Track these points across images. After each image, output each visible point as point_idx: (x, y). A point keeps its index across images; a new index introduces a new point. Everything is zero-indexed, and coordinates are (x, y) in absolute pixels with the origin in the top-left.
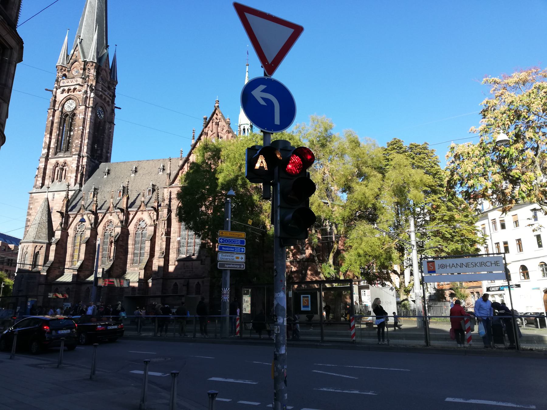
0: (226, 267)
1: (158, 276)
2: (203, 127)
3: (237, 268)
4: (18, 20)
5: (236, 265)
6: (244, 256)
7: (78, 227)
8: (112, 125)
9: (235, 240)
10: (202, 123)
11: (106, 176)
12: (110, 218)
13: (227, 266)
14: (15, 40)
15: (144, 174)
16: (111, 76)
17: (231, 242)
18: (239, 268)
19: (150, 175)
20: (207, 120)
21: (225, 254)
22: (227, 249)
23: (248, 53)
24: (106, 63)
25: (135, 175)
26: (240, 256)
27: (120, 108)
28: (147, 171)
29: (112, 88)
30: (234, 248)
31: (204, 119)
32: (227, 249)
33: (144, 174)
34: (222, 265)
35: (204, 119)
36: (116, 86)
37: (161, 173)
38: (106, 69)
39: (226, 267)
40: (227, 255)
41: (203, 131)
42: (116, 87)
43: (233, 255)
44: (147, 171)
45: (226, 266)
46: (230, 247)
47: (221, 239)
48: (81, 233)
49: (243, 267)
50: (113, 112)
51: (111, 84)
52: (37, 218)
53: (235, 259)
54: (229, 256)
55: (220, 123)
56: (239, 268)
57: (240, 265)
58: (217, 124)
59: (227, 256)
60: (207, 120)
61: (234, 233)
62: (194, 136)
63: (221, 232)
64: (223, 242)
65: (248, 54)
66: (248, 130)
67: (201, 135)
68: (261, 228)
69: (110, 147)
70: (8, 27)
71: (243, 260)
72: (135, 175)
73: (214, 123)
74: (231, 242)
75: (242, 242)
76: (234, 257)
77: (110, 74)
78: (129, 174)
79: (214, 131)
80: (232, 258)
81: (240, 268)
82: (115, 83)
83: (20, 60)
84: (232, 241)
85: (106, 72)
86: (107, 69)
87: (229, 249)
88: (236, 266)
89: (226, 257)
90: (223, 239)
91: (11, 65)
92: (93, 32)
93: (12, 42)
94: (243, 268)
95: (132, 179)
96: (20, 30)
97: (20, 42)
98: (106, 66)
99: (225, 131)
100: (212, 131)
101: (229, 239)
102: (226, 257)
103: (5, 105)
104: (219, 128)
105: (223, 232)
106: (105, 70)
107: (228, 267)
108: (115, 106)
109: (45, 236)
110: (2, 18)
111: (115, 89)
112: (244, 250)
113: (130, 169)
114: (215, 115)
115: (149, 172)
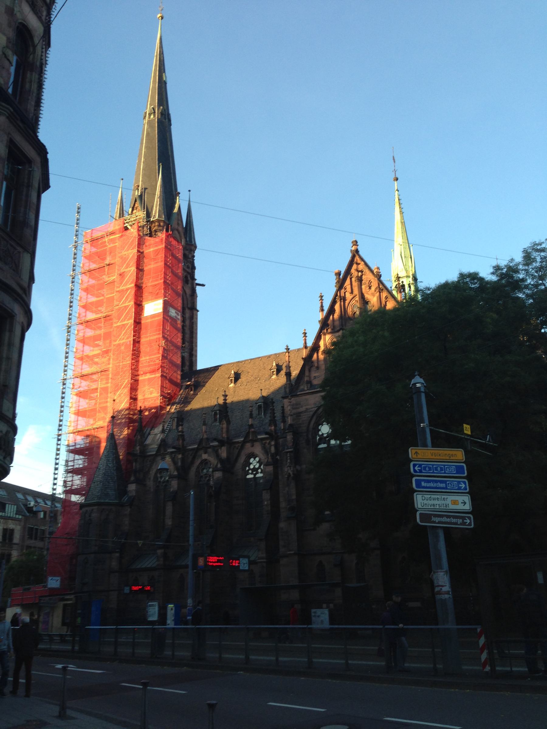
0: (434, 522)
1: (290, 551)
2: (334, 289)
3: (456, 524)
4: (40, 123)
5: (454, 517)
6: (467, 499)
7: (159, 475)
8: (195, 312)
9: (444, 465)
10: (333, 280)
11: (192, 392)
12: (205, 456)
13: (437, 520)
14: (34, 148)
15: (248, 382)
16: (186, 238)
17: (441, 468)
18: (461, 524)
19: (257, 382)
20: (341, 276)
21: (429, 496)
22: (432, 485)
23: (394, 159)
24: (178, 220)
25: (235, 385)
26: (460, 498)
27: (203, 285)
28: (252, 376)
29: (190, 256)
30: (445, 482)
31: (336, 274)
32: (432, 485)
33: (248, 382)
34: (426, 517)
35: (336, 274)
36: (194, 253)
37: (274, 377)
38: (179, 228)
39: (434, 522)
40: (433, 496)
41: (336, 295)
42: (195, 254)
43: (446, 497)
44: (252, 376)
45: (434, 519)
46: (436, 482)
47: (417, 464)
48: (164, 484)
49: (470, 522)
50: (193, 294)
51: (187, 250)
52: (101, 466)
53: (450, 505)
54: (438, 499)
55: (364, 277)
56: (461, 524)
57: (463, 518)
58: (360, 280)
59: (434, 499)
60: (341, 276)
61: (440, 452)
62: (322, 306)
63: (414, 451)
64: (420, 471)
65: (394, 162)
66: (410, 287)
67: (334, 302)
68: (489, 441)
69: (194, 347)
70: (21, 125)
71: (468, 507)
72: (235, 385)
73: (353, 279)
74: (441, 468)
75: (459, 470)
76: (449, 502)
77: (184, 235)
78: (226, 384)
79: (356, 291)
80: (443, 502)
81: (464, 524)
82: (193, 248)
83: (45, 185)
84: (439, 469)
85: (179, 233)
86: (180, 229)
87: (435, 485)
88: (454, 520)
89: (432, 502)
90: (420, 466)
91: (30, 188)
92: (156, 176)
93: (31, 153)
94: (470, 524)
95: (231, 391)
96: (43, 135)
97: (42, 151)
98: (178, 224)
99: (373, 289)
100: (352, 292)
101: (433, 465)
102: (432, 502)
103: (27, 257)
104: (363, 287)
105: (418, 451)
106: (178, 230)
107: (439, 523)
108: (197, 282)
109: (113, 492)
110: (12, 110)
111: (194, 256)
112: (464, 485)
113: (227, 376)
114: (355, 267)
115: (255, 378)
